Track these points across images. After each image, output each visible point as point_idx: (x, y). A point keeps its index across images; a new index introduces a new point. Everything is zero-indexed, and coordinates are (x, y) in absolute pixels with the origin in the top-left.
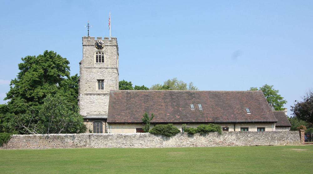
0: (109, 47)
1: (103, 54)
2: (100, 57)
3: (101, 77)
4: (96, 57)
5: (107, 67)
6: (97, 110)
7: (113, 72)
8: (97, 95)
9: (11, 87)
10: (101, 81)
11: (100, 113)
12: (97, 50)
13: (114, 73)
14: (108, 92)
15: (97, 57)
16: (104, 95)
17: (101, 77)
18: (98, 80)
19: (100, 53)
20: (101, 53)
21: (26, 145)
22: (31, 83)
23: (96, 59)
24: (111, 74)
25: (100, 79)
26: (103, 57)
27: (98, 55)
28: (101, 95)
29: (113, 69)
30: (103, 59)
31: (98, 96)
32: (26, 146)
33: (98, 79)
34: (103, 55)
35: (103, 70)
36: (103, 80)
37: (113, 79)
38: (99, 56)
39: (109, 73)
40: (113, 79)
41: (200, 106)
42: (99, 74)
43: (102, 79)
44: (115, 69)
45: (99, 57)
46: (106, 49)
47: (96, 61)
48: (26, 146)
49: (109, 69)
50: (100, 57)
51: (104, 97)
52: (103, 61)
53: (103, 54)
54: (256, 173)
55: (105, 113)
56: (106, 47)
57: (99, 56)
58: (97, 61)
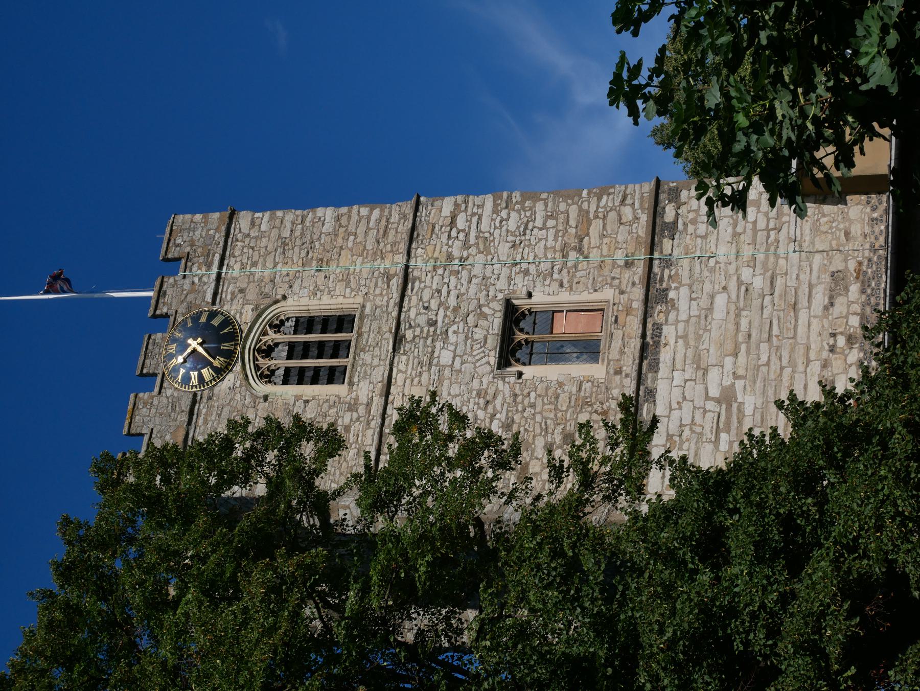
0: (234, 270)
1: (278, 327)
2: (305, 350)
3: (479, 334)
4: (300, 382)
5: (396, 283)
6: (816, 367)
7: (453, 224)
8: (655, 367)
9: (617, 7)
10: (520, 336)
11: (850, 340)
12: (238, 368)
13: (461, 222)
14: (628, 264)
15: (301, 377)
17: (479, 334)
18: (504, 361)
19: (268, 352)
20: (272, 336)
22: (125, 590)
23: (315, 381)
25: (494, 342)
26: (307, 324)
27: (280, 361)
28: (658, 327)
29: (423, 230)
31: (665, 356)
34: (283, 351)
35: (422, 320)
37: (512, 225)
38: (290, 357)
39: (450, 257)
40: (512, 225)
42: (445, 357)
45: (305, 356)
46: (242, 291)
47: (330, 381)
49: (418, 263)
50: (305, 350)
52: (343, 322)
53: (278, 327)
55: (854, 288)
56: (228, 290)
57: (290, 357)
58: (334, 376)
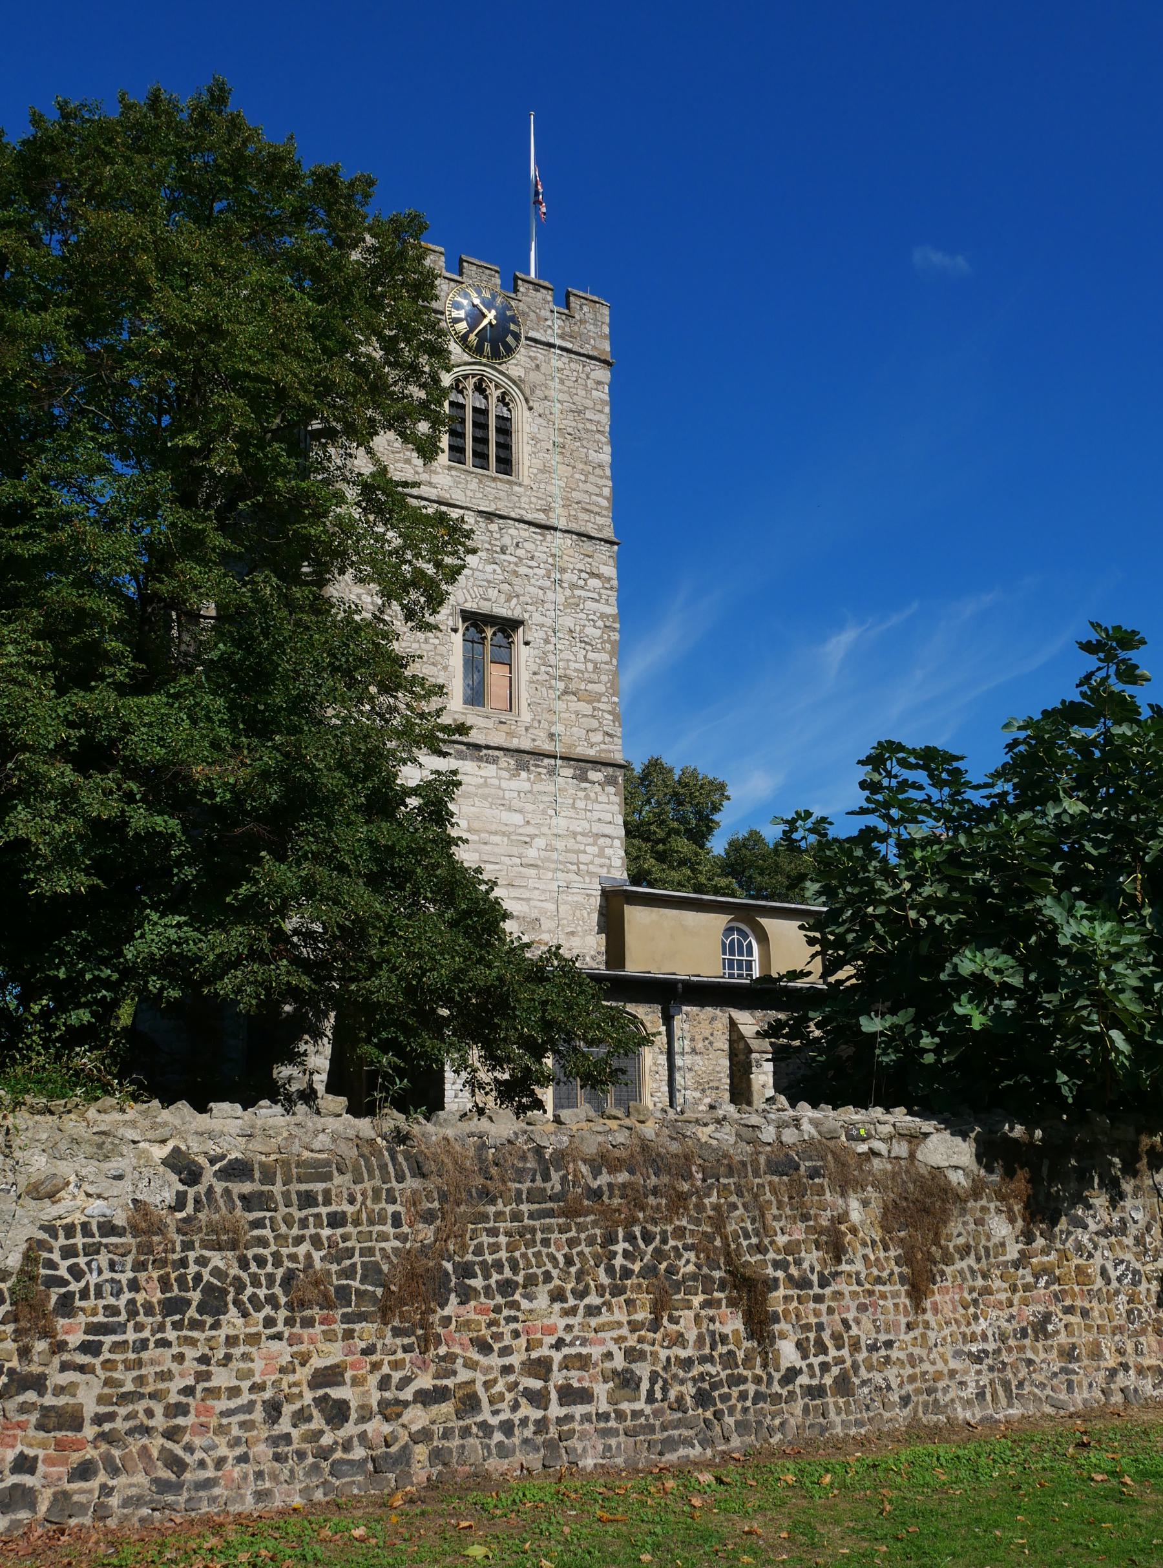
2: (481, 426)
10: (489, 632)
12: (467, 358)
14: (551, 736)
16: (523, 767)
17: (492, 593)
19: (480, 389)
21: (1041, 1328)
24: (573, 586)
25: (485, 607)
26: (505, 428)
28: (495, 761)
29: (588, 546)
30: (505, 447)
32: (1047, 1359)
33: (468, 606)
35: (507, 540)
36: (508, 626)
37: (590, 630)
39: (563, 570)
40: (590, 630)
41: (1038, 1133)
43: (502, 610)
44: (605, 547)
48: (1047, 1359)
49: (558, 541)
50: (481, 426)
51: (514, 784)
52: (506, 464)
54: (64, 1567)
